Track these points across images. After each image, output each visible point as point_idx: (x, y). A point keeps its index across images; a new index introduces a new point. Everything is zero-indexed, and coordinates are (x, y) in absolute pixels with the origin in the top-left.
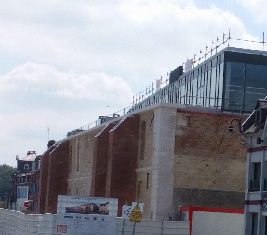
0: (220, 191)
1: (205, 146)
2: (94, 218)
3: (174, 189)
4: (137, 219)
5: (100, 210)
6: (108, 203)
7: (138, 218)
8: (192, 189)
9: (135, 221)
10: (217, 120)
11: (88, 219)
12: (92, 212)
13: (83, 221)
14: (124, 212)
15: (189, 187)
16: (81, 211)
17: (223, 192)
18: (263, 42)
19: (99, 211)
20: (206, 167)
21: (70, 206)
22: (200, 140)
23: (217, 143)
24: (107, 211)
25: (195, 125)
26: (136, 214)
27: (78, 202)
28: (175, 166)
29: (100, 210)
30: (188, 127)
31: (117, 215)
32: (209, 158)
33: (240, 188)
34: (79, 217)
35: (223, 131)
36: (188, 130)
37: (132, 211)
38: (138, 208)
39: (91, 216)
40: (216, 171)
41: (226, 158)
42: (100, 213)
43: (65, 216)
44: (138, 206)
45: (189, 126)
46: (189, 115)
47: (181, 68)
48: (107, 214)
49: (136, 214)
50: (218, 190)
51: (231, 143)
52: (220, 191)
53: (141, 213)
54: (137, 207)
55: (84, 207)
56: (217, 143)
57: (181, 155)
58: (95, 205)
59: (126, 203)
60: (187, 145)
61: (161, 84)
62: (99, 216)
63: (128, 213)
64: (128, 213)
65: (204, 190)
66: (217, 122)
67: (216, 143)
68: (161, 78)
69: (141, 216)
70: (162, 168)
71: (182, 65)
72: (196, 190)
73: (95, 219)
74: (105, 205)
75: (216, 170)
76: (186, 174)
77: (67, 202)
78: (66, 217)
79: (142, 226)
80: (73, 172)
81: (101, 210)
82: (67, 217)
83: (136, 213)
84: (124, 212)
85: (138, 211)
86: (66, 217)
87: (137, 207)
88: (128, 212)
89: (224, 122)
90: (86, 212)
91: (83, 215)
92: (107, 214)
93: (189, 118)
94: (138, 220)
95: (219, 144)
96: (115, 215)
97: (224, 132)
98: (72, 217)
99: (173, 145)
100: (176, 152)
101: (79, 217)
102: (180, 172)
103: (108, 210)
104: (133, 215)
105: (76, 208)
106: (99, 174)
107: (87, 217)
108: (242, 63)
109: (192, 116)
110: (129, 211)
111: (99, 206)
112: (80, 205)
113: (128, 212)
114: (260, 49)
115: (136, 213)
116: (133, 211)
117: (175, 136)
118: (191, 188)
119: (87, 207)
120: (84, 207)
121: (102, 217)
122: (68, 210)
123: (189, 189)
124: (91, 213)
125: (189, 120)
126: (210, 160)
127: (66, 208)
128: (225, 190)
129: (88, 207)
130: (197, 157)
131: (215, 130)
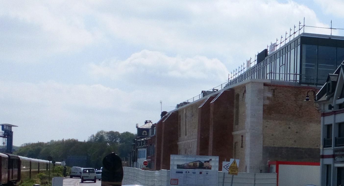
2: (200, 172)
4: (234, 173)
7: (235, 172)
9: (233, 173)
12: (197, 167)
14: (224, 167)
16: (190, 167)
17: (303, 149)
21: (181, 163)
24: (210, 166)
26: (234, 168)
27: (187, 160)
28: (263, 129)
29: (205, 166)
37: (230, 166)
38: (235, 163)
39: (198, 171)
40: (297, 132)
43: (182, 173)
44: (234, 162)
46: (274, 88)
47: (266, 51)
49: (234, 168)
51: (308, 109)
53: (237, 167)
55: (192, 164)
58: (200, 162)
59: (225, 160)
61: (251, 63)
62: (204, 171)
63: (227, 168)
64: (227, 168)
65: (287, 148)
71: (266, 48)
74: (208, 162)
76: (273, 135)
77: (178, 160)
80: (182, 136)
82: (179, 172)
85: (235, 166)
88: (227, 167)
91: (191, 170)
92: (211, 169)
99: (261, 112)
100: (264, 118)
101: (187, 172)
105: (185, 165)
106: (203, 137)
107: (194, 172)
110: (227, 166)
113: (227, 167)
118: (277, 146)
120: (192, 164)
122: (179, 167)
125: (274, 92)
126: (291, 123)
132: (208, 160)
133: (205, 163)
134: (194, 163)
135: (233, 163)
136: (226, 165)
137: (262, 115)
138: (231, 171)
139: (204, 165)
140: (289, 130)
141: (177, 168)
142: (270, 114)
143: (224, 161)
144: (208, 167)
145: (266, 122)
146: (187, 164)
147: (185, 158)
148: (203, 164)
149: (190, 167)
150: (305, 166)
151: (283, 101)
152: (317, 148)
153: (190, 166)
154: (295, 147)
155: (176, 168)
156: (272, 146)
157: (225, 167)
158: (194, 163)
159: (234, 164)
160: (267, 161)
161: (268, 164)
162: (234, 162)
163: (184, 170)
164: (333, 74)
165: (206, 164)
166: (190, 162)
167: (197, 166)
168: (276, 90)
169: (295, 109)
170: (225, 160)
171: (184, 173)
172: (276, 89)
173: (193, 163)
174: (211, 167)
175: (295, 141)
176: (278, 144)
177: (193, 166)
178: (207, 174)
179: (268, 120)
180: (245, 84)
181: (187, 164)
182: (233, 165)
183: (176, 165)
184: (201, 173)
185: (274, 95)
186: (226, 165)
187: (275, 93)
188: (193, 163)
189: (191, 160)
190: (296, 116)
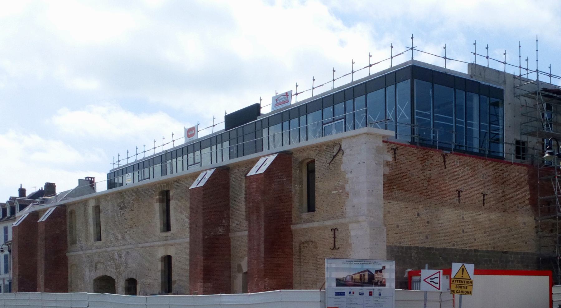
0: (434, 248)
1: (413, 189)
2: (370, 292)
3: (387, 247)
4: (464, 290)
5: (376, 280)
6: (384, 267)
7: (466, 288)
8: (405, 247)
9: (462, 292)
10: (423, 155)
11: (363, 294)
12: (366, 283)
13: (356, 298)
14: (424, 280)
15: (401, 245)
16: (355, 283)
17: (437, 250)
18: (445, 58)
19: (375, 281)
20: (416, 216)
21: (342, 275)
22: (408, 180)
23: (425, 185)
24: (384, 281)
25: (401, 160)
26: (462, 282)
27: (350, 269)
28: (385, 216)
29: (376, 280)
30: (394, 163)
31: (394, 287)
32: (419, 204)
33: (452, 243)
34: (352, 293)
35: (429, 169)
36: (394, 167)
38: (465, 271)
39: (366, 289)
40: (428, 222)
41: (435, 204)
42: (376, 284)
43: (344, 295)
44: (463, 269)
45: (395, 161)
46: (394, 147)
47: (257, 107)
48: (384, 285)
49: (462, 282)
50: (431, 247)
51: (438, 184)
52: (432, 249)
53: (470, 279)
54: (463, 270)
55: (357, 277)
56: (425, 185)
57: (391, 201)
58: (370, 273)
59: (427, 266)
60: (394, 187)
61: (198, 131)
62: (375, 289)
63: (431, 282)
64: (431, 282)
65: (417, 247)
66: (422, 156)
67: (423, 185)
68: (198, 124)
69: (470, 284)
70: (372, 219)
71: (259, 103)
72: (410, 248)
73: (371, 294)
74: (380, 271)
75: (427, 220)
76: (398, 226)
77: (337, 269)
78: (338, 294)
79: (408, 301)
80: (81, 242)
81: (376, 280)
82: (340, 293)
83: (462, 280)
84: (424, 280)
85: (465, 276)
86: (338, 294)
87: (463, 270)
89: (429, 157)
90: (359, 284)
91: (357, 289)
92: (384, 285)
93: (395, 150)
94: (467, 290)
95: (427, 186)
96: (392, 286)
97: (430, 171)
98: (344, 293)
99: (381, 187)
100: (386, 197)
101: (352, 293)
102: (391, 224)
103: (385, 279)
104: (456, 283)
105: (348, 279)
106: (206, 237)
107: (361, 292)
108: (430, 82)
109: (397, 148)
110: (432, 277)
111: (374, 274)
112: (352, 273)
114: (443, 66)
115: (462, 280)
116: (455, 277)
117: (382, 175)
118: (404, 245)
119: (361, 275)
120: (357, 277)
121: (379, 290)
122: (340, 282)
123: (402, 248)
124: (368, 285)
125: (395, 153)
126: (420, 207)
127: (337, 279)
128: (438, 247)
129: (362, 275)
130: (407, 203)
131: (421, 167)
132: (380, 267)
133: (376, 274)
134: (361, 274)
135: (461, 270)
136: (430, 277)
137: (382, 192)
138: (457, 287)
139: (375, 277)
140: (418, 218)
141: (337, 285)
142: (392, 191)
143: (424, 269)
144: (381, 282)
145: (389, 205)
146: (350, 276)
147: (347, 266)
148: (374, 275)
149: (354, 282)
150: (505, 276)
151: (407, 170)
152: (453, 247)
153: (355, 280)
154: (427, 246)
155: (334, 284)
156: (398, 245)
157: (428, 280)
158: (361, 274)
159: (463, 274)
160: (407, 269)
161: (406, 275)
162: (463, 269)
163: (346, 289)
164: (463, 127)
165: (378, 275)
166: (354, 273)
167: (365, 281)
168: (398, 150)
169: (423, 184)
170: (427, 266)
171: (347, 294)
172: (397, 148)
173: (359, 275)
174: (385, 282)
175: (427, 237)
176: (405, 242)
177: (360, 281)
178: (380, 295)
179: (391, 201)
180: (342, 139)
181: (351, 277)
182: (459, 276)
183: (335, 280)
184: (371, 294)
185: (395, 158)
186: (430, 277)
187: (483, 144)
188: (359, 275)
189: (354, 269)
190: (424, 195)
